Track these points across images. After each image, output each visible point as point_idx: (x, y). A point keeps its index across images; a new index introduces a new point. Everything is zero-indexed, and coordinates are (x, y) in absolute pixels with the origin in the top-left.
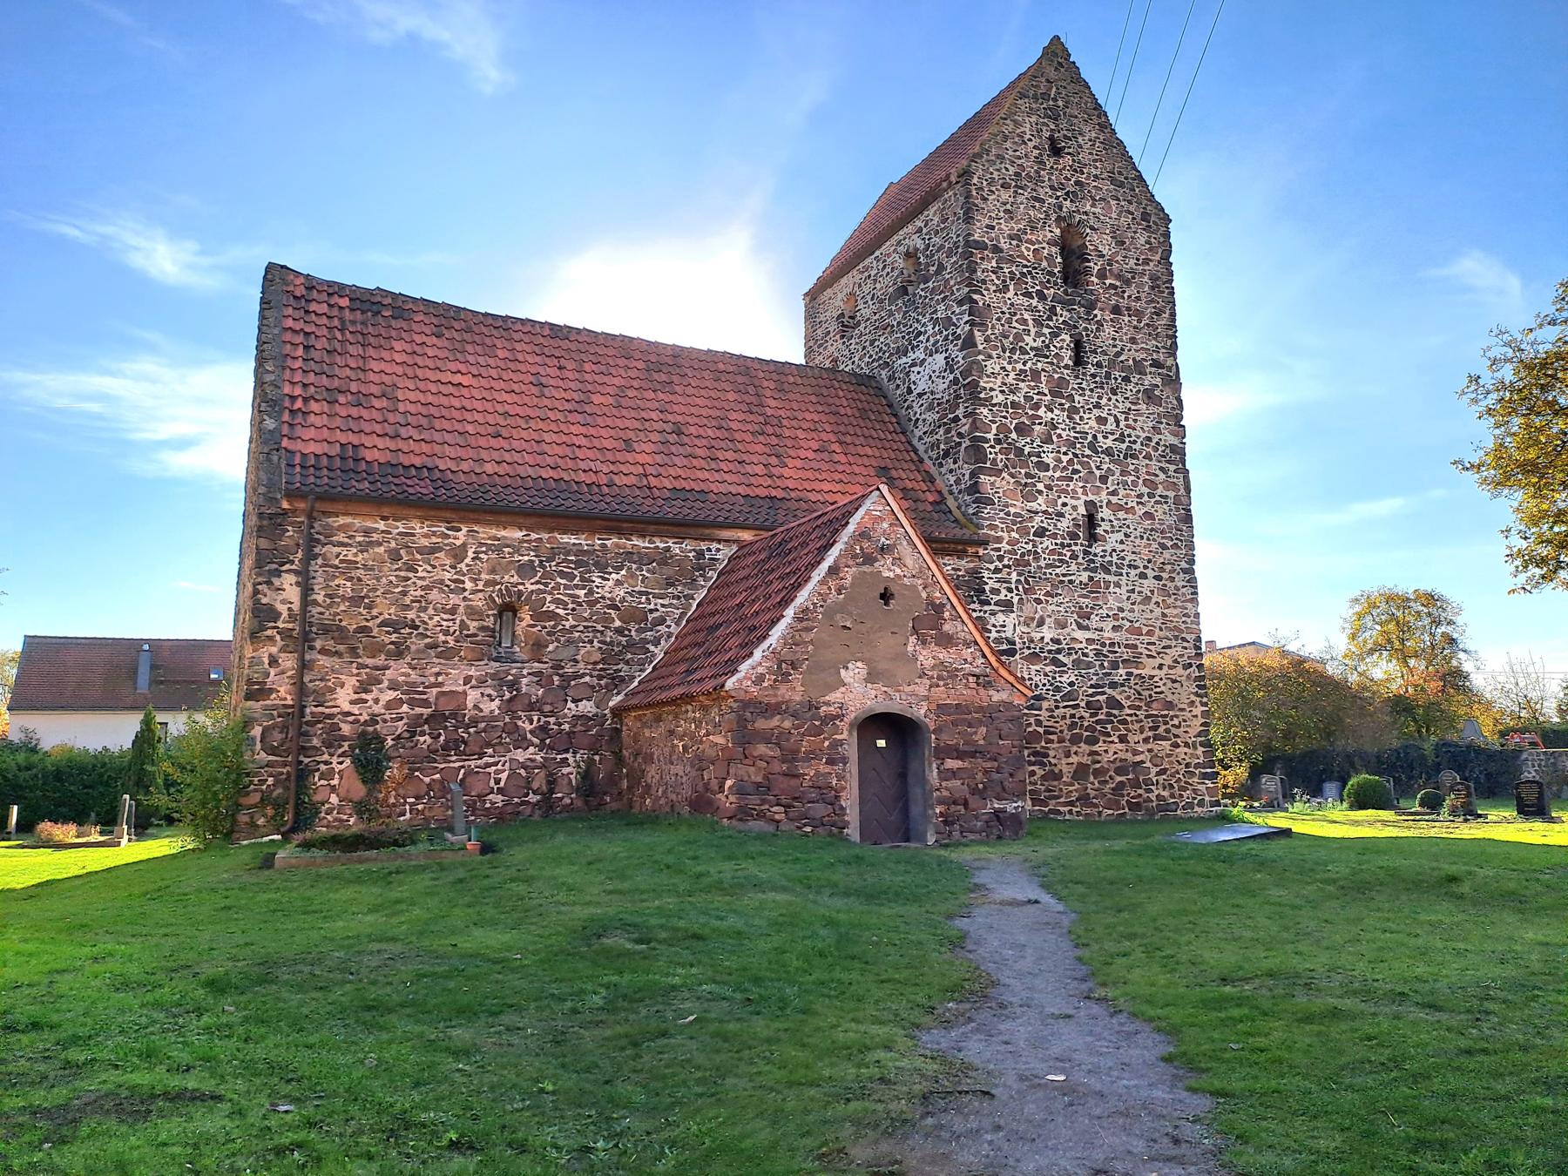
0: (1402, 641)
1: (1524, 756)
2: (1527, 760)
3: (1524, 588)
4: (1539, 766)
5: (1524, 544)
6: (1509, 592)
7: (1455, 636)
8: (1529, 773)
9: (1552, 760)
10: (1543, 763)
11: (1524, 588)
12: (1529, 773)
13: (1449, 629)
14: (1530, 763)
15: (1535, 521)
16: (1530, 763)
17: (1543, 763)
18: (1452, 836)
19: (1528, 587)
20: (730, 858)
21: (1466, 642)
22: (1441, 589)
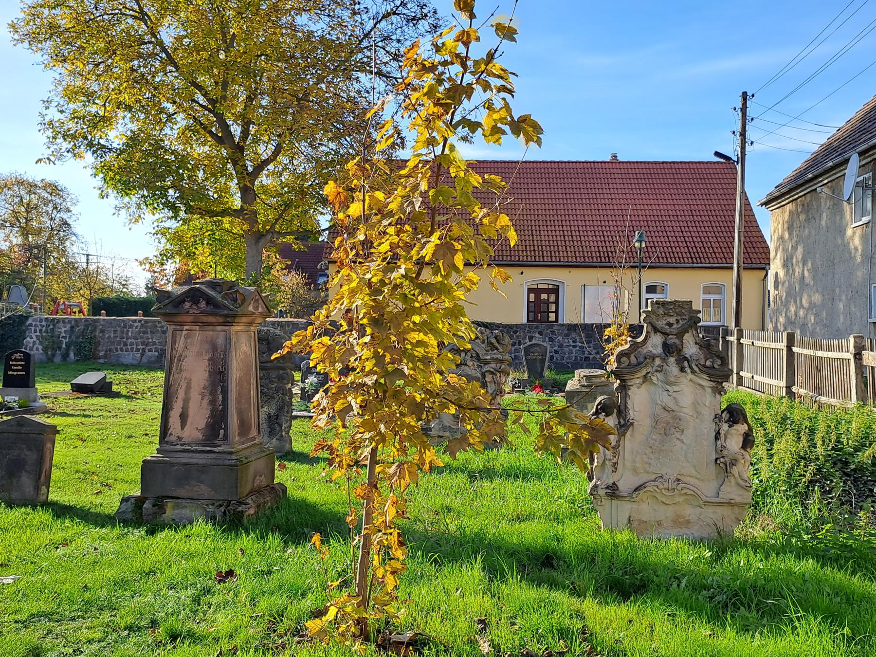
0: (28, 221)
1: (29, 321)
2: (31, 325)
3: (48, 159)
4: (41, 331)
5: (58, 116)
6: (37, 162)
7: (69, 221)
8: (31, 338)
9: (51, 327)
10: (44, 329)
11: (48, 159)
12: (31, 338)
13: (64, 216)
14: (33, 328)
15: (71, 94)
16: (33, 328)
17: (44, 329)
18: (590, 370)
19: (52, 158)
20: (114, 374)
21: (76, 227)
22: (62, 182)
